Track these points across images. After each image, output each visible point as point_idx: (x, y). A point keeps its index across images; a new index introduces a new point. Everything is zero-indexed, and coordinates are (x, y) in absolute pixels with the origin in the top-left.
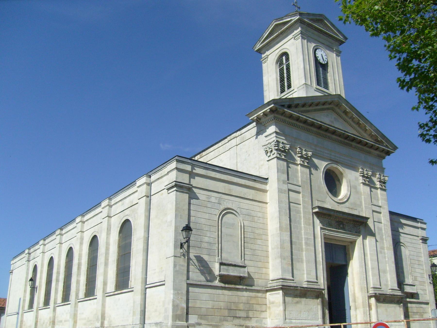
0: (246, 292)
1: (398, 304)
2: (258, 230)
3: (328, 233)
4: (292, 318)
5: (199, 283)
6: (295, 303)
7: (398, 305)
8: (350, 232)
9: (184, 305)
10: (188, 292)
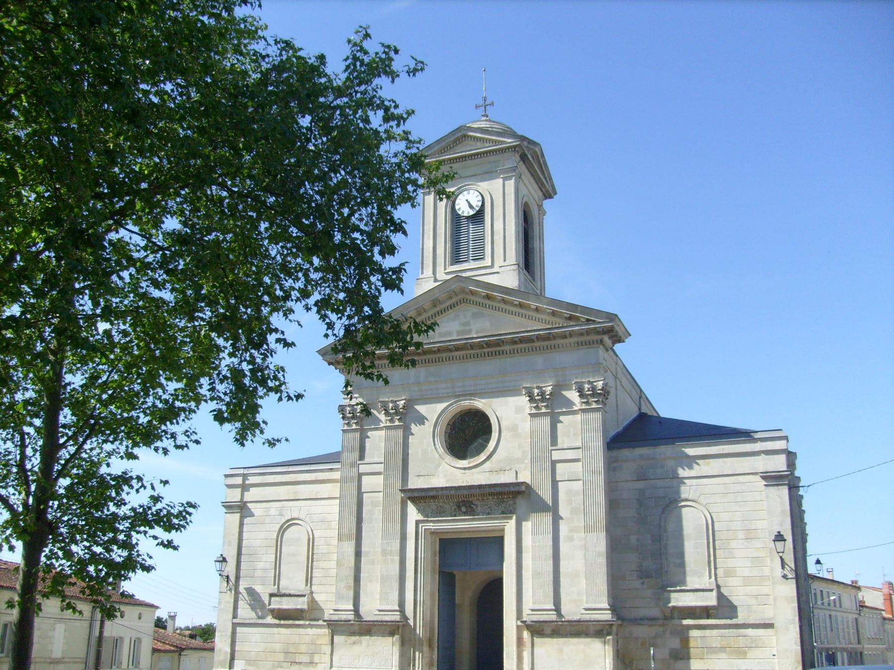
1: (601, 638)
5: (247, 622)
6: (350, 644)
9: (228, 649)
10: (234, 633)
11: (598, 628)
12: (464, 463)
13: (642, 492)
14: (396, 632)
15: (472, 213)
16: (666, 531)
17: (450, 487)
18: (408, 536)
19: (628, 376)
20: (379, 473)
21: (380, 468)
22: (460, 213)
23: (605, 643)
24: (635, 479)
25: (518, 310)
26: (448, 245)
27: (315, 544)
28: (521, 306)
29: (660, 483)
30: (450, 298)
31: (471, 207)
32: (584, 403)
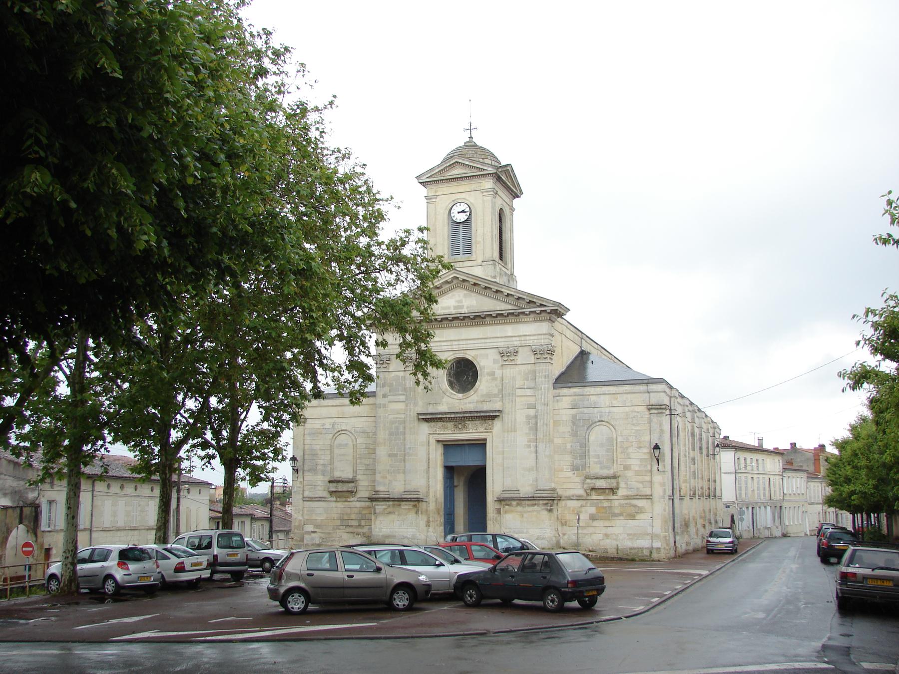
13: (575, 416)
19: (572, 328)
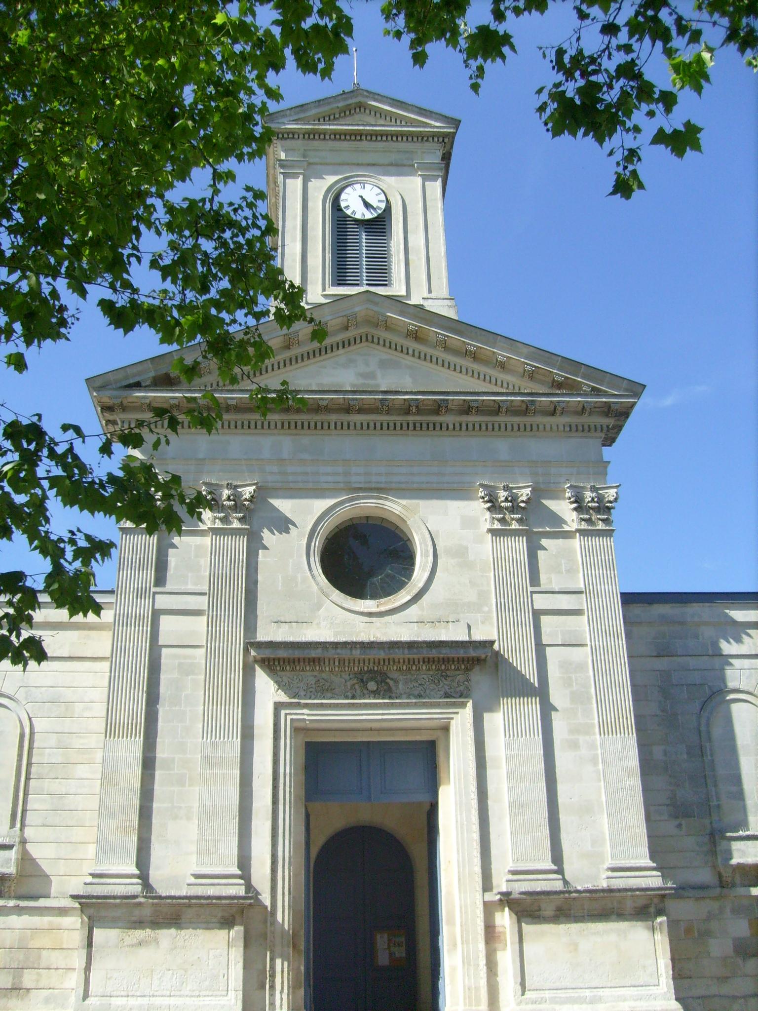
0: (19, 915)
2: (80, 737)
3: (308, 715)
4: (115, 993)
6: (129, 946)
7: (639, 923)
8: (420, 696)
11: (641, 902)
12: (368, 605)
14: (238, 919)
15: (369, 215)
16: (710, 739)
17: (353, 643)
18: (256, 731)
20: (197, 613)
21: (201, 603)
22: (349, 212)
23: (653, 929)
24: (655, 654)
25: (467, 363)
26: (329, 256)
27: (36, 745)
28: (475, 356)
29: (692, 662)
30: (346, 328)
31: (367, 205)
32: (583, 520)
